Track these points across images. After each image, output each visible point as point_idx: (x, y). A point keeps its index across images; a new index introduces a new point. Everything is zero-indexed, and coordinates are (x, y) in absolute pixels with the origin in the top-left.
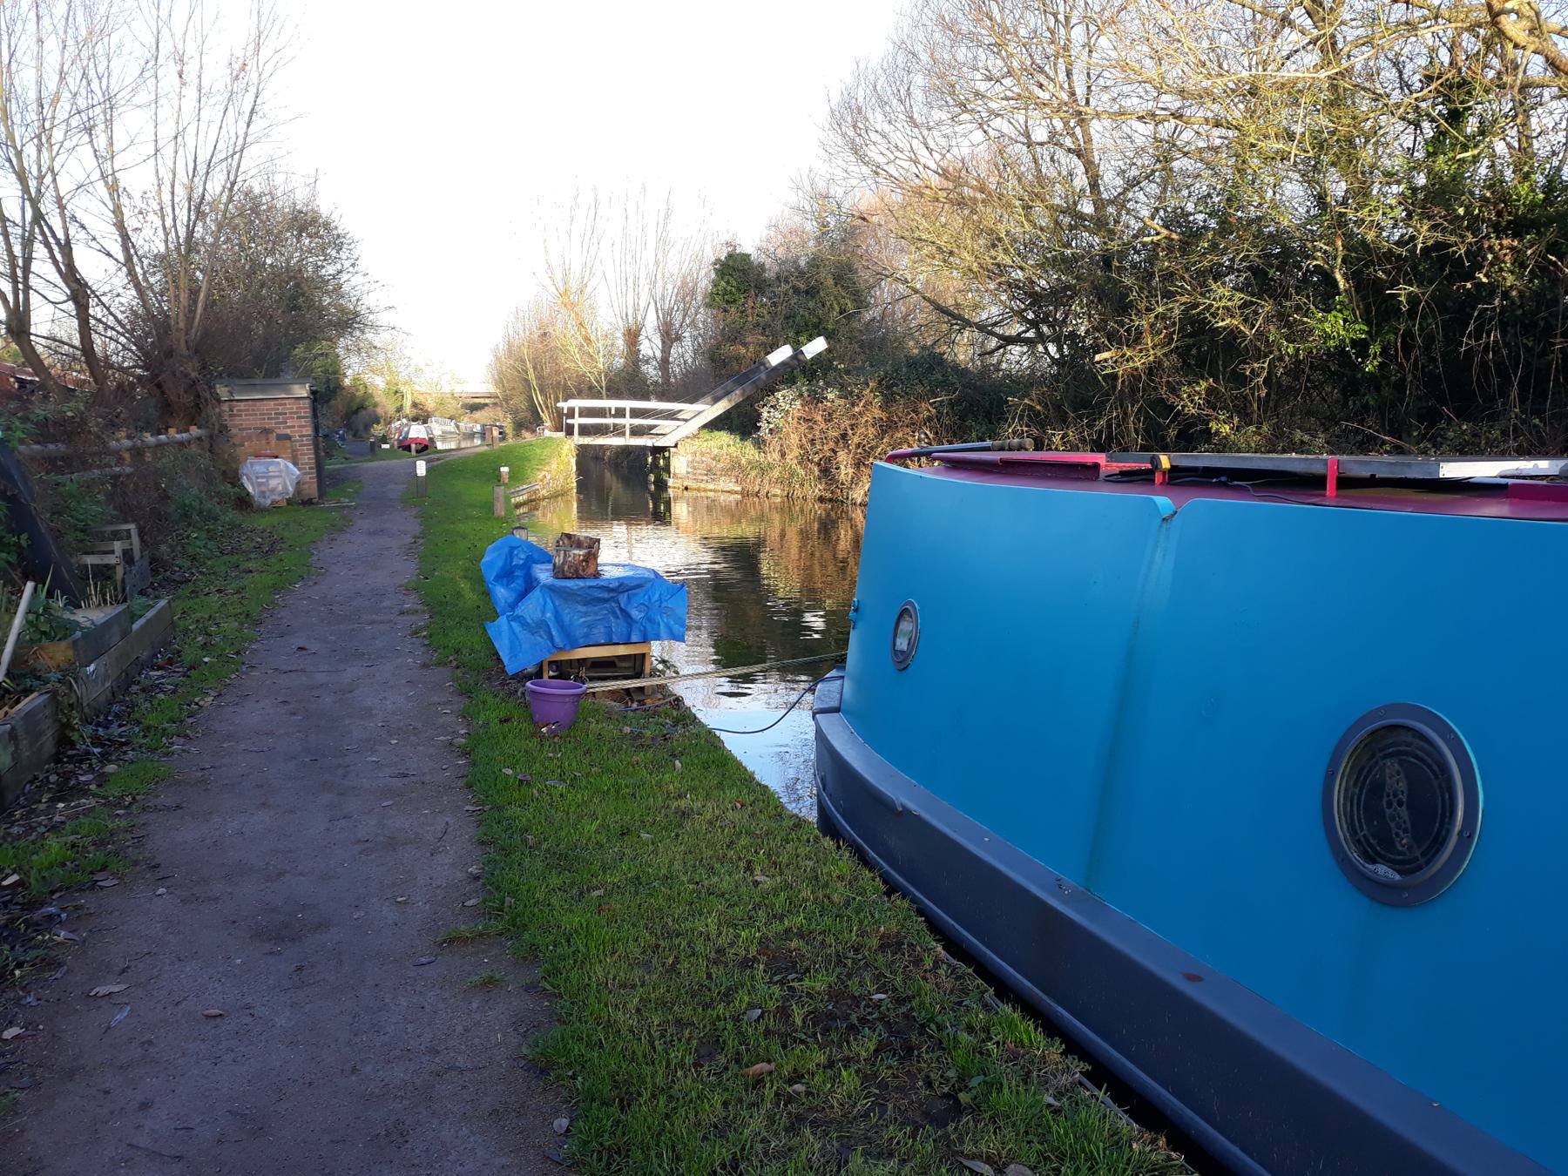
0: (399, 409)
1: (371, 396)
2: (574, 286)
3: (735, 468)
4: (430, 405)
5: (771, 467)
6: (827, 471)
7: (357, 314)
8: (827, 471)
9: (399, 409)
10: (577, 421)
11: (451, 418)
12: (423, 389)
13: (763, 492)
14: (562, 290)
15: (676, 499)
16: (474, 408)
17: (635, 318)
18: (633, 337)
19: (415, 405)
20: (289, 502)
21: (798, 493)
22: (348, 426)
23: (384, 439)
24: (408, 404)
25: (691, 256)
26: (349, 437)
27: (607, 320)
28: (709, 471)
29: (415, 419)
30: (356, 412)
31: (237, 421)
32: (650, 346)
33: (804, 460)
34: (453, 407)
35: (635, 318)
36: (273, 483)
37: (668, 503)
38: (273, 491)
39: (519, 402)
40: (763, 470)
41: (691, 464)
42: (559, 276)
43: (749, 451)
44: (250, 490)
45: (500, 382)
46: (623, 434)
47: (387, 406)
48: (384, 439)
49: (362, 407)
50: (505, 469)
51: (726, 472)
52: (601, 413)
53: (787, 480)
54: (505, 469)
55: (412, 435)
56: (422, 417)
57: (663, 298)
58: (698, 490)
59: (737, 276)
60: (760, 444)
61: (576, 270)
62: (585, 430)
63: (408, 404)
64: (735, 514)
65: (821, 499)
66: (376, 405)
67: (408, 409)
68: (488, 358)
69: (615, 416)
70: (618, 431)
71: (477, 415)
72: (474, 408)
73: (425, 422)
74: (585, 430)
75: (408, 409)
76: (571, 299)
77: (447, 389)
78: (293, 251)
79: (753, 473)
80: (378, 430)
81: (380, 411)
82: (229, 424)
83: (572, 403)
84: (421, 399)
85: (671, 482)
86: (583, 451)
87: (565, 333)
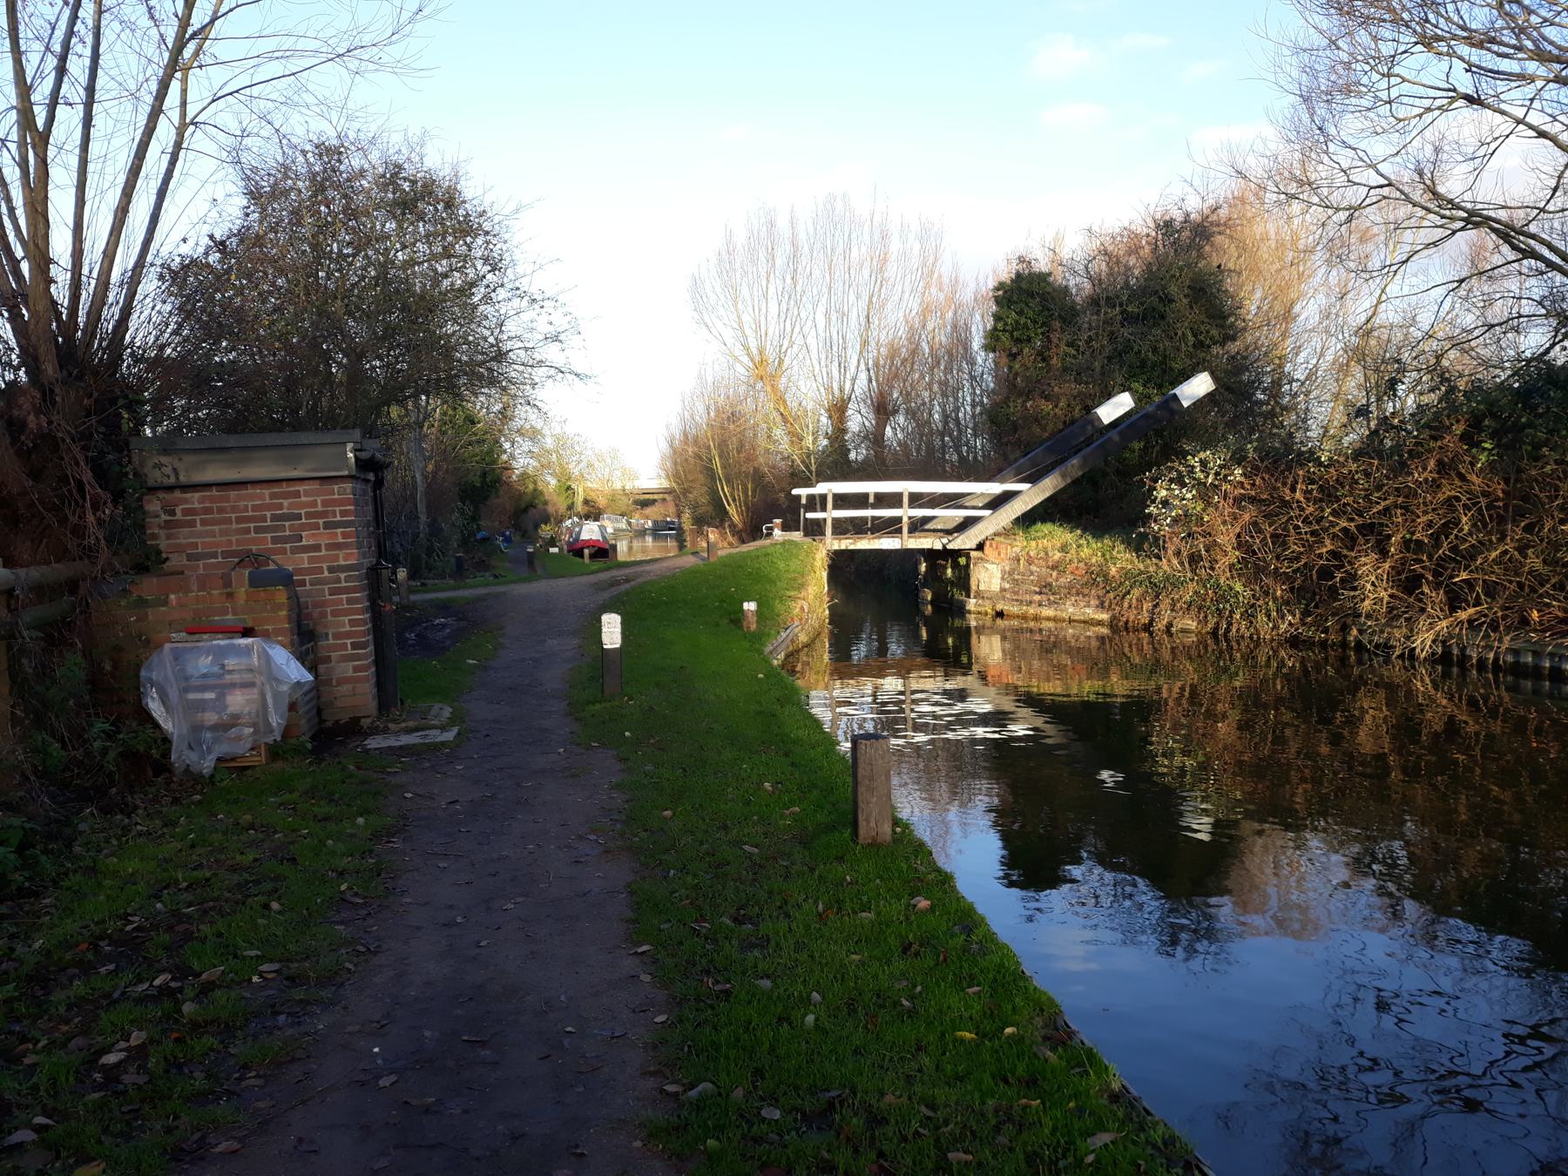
0: (570, 507)
1: (541, 493)
2: (771, 355)
3: (1096, 581)
4: (602, 502)
5: (1173, 583)
6: (1320, 588)
7: (501, 356)
8: (1320, 588)
9: (570, 507)
10: (832, 514)
11: (623, 515)
12: (594, 486)
13: (1160, 625)
14: (757, 359)
15: (980, 630)
16: (644, 504)
17: (841, 390)
18: (838, 410)
19: (586, 502)
20: (275, 752)
21: (1240, 626)
22: (517, 527)
23: (552, 542)
24: (579, 499)
25: (980, 263)
26: (516, 538)
27: (808, 390)
28: (1045, 588)
29: (587, 517)
30: (525, 510)
31: (183, 537)
32: (858, 420)
33: (1250, 567)
34: (624, 503)
35: (841, 390)
36: (238, 701)
37: (964, 635)
38: (234, 721)
39: (699, 494)
40: (1156, 590)
41: (1007, 575)
42: (753, 344)
43: (1122, 559)
44: (167, 725)
45: (676, 476)
46: (899, 531)
47: (559, 503)
48: (552, 542)
49: (531, 505)
50: (750, 606)
51: (1075, 591)
52: (860, 501)
53: (1215, 602)
54: (750, 606)
55: (584, 536)
56: (593, 513)
57: (876, 365)
58: (1024, 617)
59: (1027, 301)
60: (1144, 544)
61: (773, 329)
62: (841, 528)
63: (579, 499)
64: (1099, 657)
65: (1294, 642)
66: (546, 503)
67: (579, 507)
68: (664, 447)
69: (874, 506)
70: (891, 527)
71: (648, 511)
72: (644, 504)
73: (596, 519)
74: (841, 528)
75: (579, 507)
76: (766, 372)
77: (618, 486)
78: (410, 250)
79: (1136, 592)
80: (546, 531)
81: (550, 509)
82: (163, 544)
83: (822, 488)
84: (593, 496)
85: (971, 604)
86: (841, 564)
87: (757, 409)
